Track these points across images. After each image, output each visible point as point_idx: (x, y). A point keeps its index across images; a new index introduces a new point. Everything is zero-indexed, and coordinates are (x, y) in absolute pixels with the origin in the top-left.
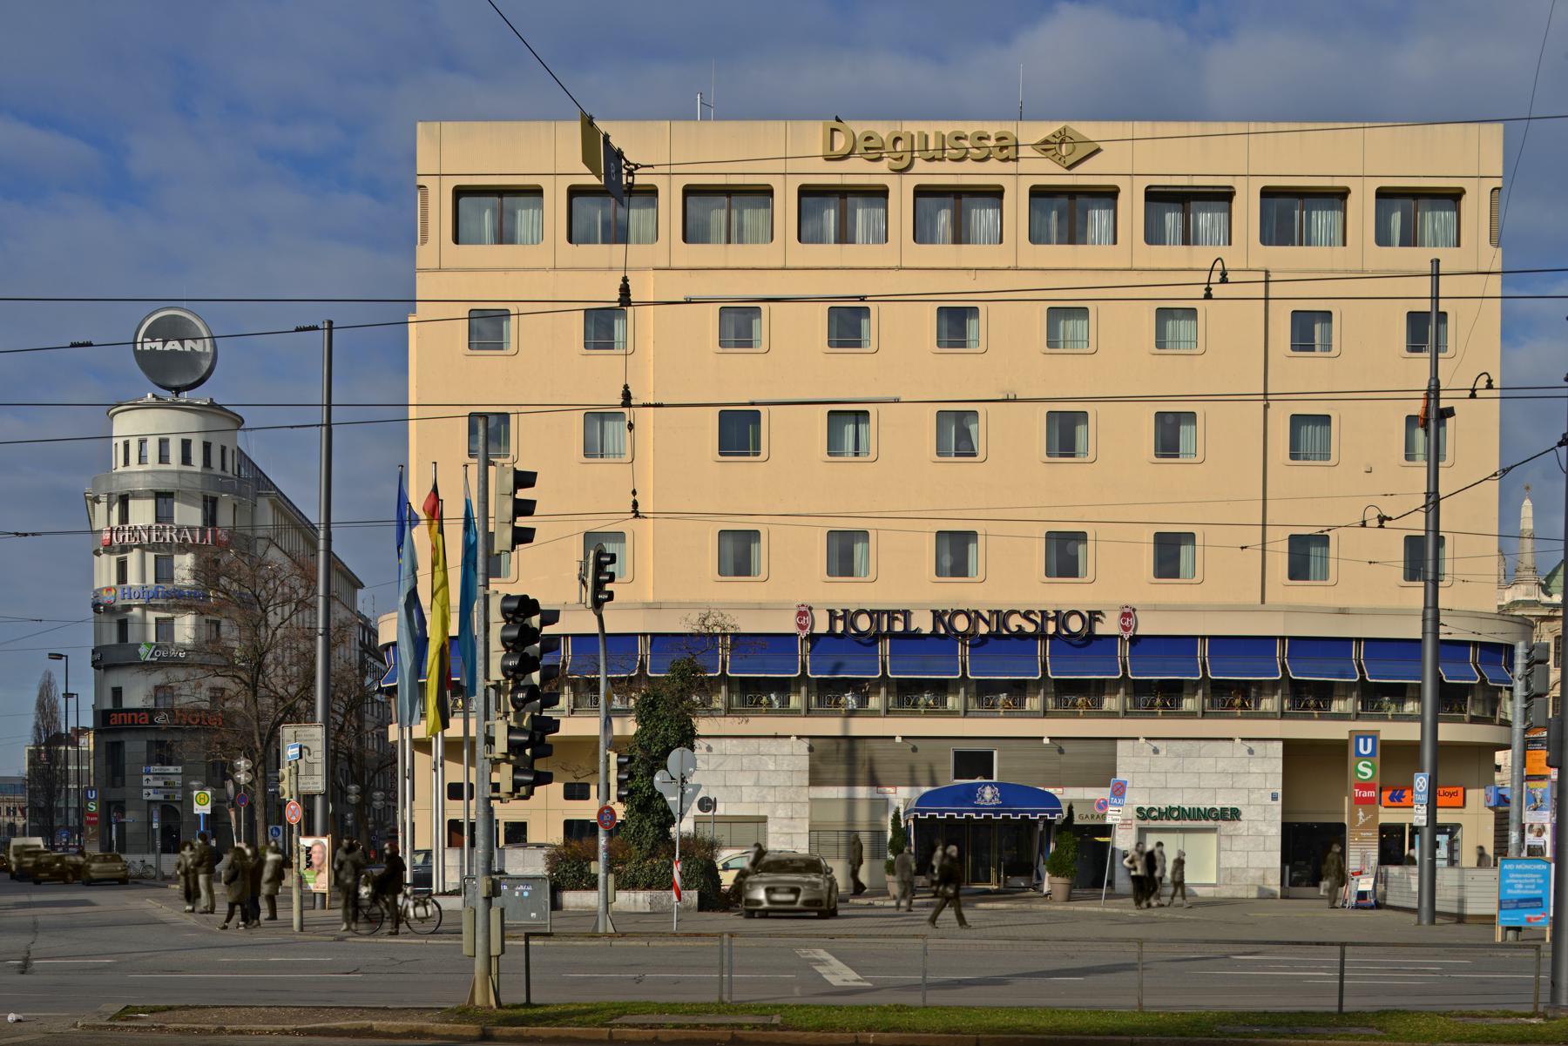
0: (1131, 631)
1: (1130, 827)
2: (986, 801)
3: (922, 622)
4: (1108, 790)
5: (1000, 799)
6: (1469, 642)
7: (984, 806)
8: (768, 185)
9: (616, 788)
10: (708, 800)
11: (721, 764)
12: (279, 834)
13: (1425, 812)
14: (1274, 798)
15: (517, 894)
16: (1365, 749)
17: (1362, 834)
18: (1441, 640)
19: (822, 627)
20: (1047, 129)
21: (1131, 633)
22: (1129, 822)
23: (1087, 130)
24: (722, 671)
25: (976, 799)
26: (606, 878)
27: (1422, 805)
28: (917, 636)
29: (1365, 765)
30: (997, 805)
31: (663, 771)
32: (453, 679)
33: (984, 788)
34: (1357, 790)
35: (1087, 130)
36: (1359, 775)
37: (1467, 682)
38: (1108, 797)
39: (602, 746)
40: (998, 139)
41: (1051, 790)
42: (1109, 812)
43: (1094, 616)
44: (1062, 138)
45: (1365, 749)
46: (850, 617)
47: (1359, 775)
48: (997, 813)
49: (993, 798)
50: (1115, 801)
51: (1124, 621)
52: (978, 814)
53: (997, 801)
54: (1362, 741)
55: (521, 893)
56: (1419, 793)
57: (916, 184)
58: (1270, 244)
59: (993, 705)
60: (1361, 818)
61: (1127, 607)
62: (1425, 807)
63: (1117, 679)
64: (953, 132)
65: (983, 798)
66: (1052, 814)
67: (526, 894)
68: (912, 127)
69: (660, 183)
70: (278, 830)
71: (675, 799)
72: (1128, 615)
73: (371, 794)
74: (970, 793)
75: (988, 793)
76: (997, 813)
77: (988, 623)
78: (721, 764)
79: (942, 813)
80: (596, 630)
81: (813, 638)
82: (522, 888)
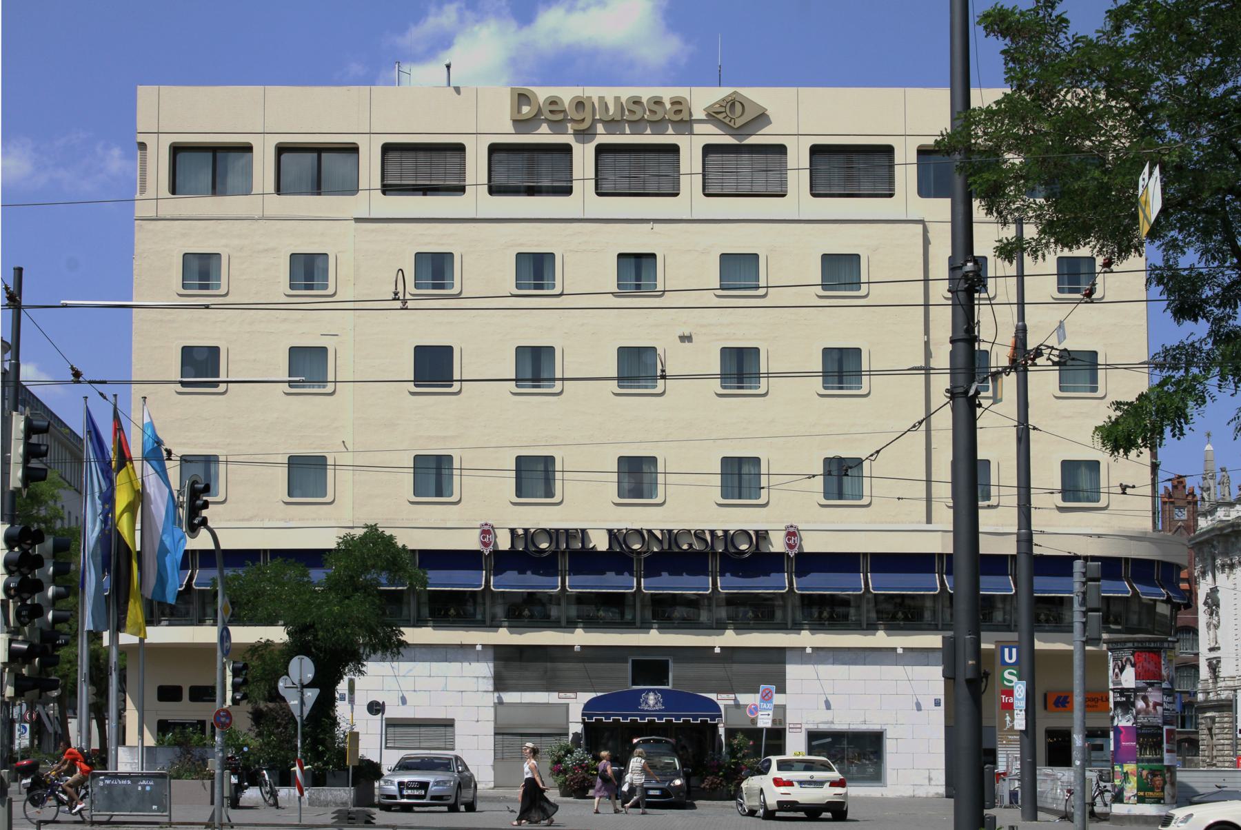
0: (796, 549)
1: (799, 730)
2: (649, 706)
3: (600, 543)
4: (758, 696)
5: (663, 705)
6: (930, 557)
7: (647, 711)
8: (354, 143)
9: (231, 693)
10: (377, 703)
11: (411, 670)
12: (26, 730)
13: (1024, 717)
14: (937, 703)
15: (140, 788)
16: (1010, 658)
17: (1010, 737)
18: (1042, 558)
19: (504, 543)
20: (716, 94)
21: (796, 550)
22: (799, 726)
23: (756, 95)
24: (562, 587)
25: (640, 705)
26: (222, 774)
27: (1021, 711)
28: (594, 553)
29: (1010, 673)
30: (660, 710)
31: (285, 677)
32: (1035, 595)
33: (647, 694)
34: (1003, 696)
35: (756, 95)
36: (1005, 683)
37: (922, 593)
38: (758, 703)
39: (219, 654)
40: (673, 104)
41: (713, 696)
42: (760, 717)
43: (762, 535)
44: (732, 103)
45: (1010, 658)
46: (529, 536)
47: (1005, 683)
48: (660, 717)
49: (656, 703)
50: (765, 706)
51: (789, 540)
52: (643, 717)
53: (659, 707)
54: (1006, 650)
55: (143, 787)
56: (1018, 699)
57: (278, 142)
58: (928, 196)
59: (668, 617)
60: (1008, 722)
61: (792, 526)
62: (1023, 712)
63: (860, 595)
64: (574, 98)
65: (646, 703)
66: (713, 718)
67: (148, 788)
68: (593, 93)
69: (149, 140)
70: (25, 728)
71: (296, 702)
72: (792, 533)
73: (1201, 702)
74: (633, 700)
75: (651, 699)
76: (660, 717)
77: (661, 542)
78: (411, 670)
79: (695, 718)
80: (212, 546)
81: (497, 554)
82: (144, 782)
